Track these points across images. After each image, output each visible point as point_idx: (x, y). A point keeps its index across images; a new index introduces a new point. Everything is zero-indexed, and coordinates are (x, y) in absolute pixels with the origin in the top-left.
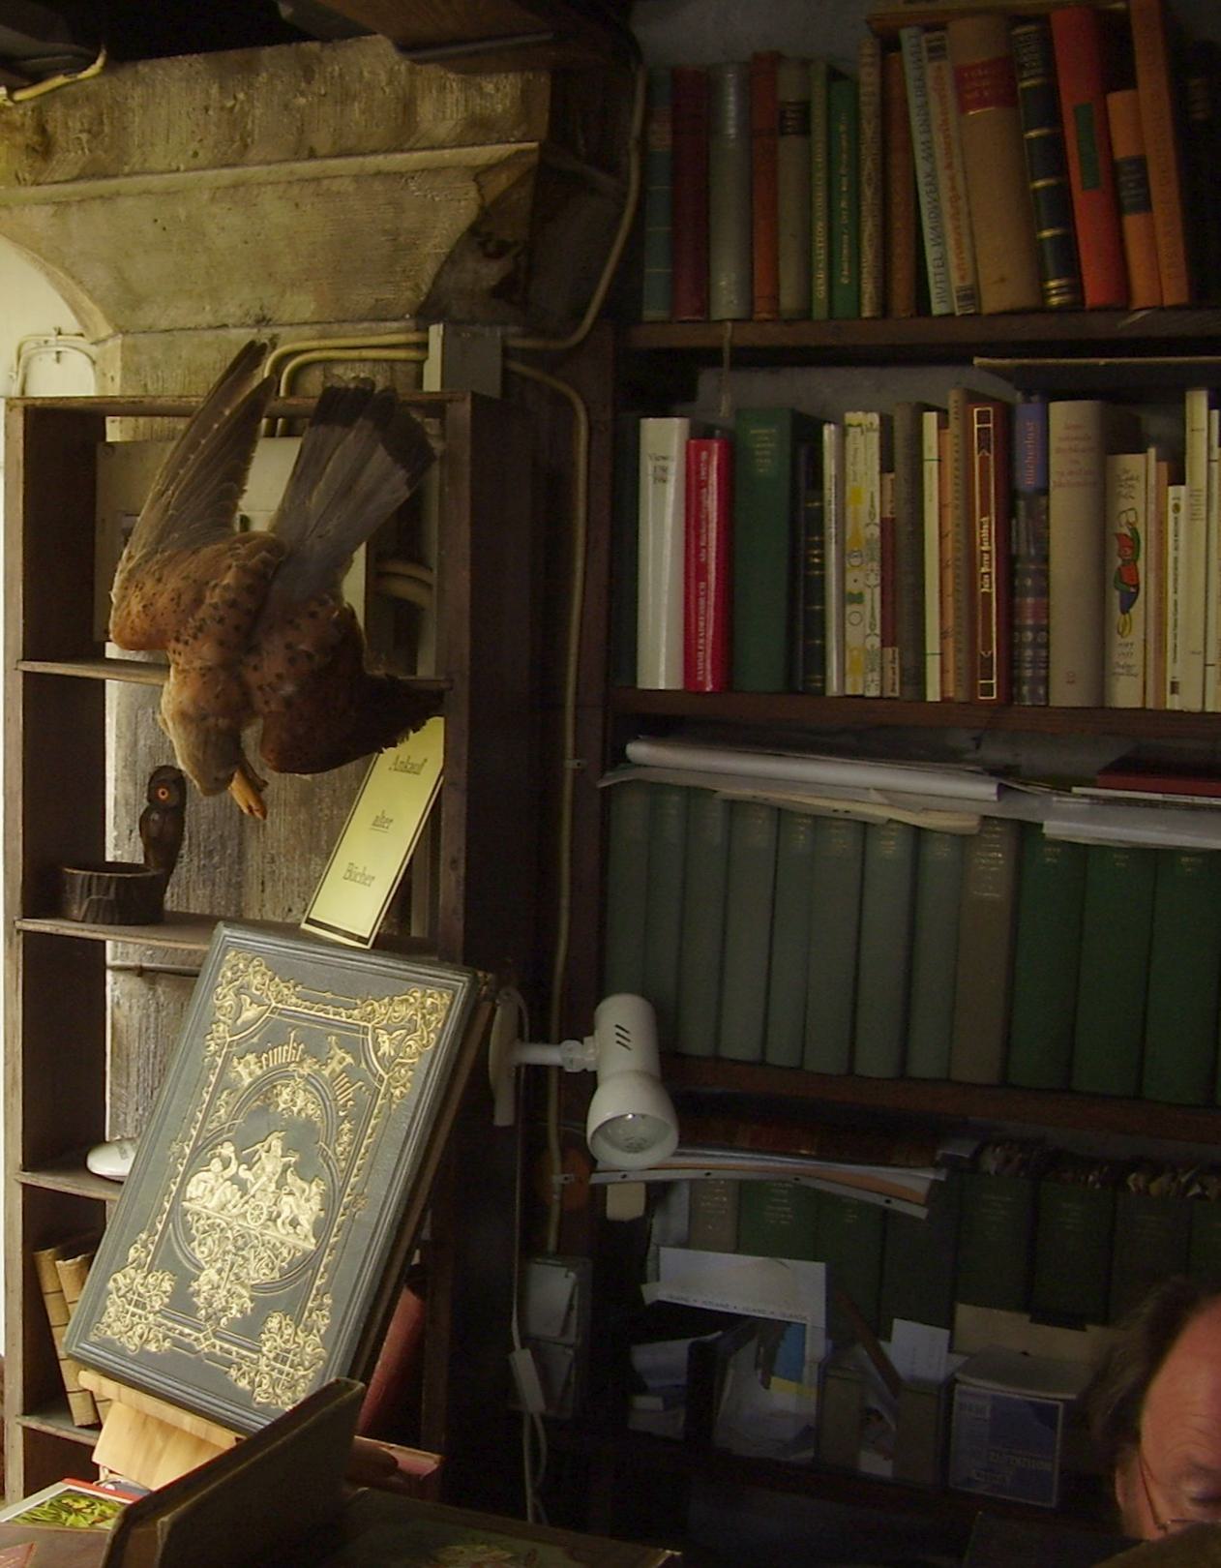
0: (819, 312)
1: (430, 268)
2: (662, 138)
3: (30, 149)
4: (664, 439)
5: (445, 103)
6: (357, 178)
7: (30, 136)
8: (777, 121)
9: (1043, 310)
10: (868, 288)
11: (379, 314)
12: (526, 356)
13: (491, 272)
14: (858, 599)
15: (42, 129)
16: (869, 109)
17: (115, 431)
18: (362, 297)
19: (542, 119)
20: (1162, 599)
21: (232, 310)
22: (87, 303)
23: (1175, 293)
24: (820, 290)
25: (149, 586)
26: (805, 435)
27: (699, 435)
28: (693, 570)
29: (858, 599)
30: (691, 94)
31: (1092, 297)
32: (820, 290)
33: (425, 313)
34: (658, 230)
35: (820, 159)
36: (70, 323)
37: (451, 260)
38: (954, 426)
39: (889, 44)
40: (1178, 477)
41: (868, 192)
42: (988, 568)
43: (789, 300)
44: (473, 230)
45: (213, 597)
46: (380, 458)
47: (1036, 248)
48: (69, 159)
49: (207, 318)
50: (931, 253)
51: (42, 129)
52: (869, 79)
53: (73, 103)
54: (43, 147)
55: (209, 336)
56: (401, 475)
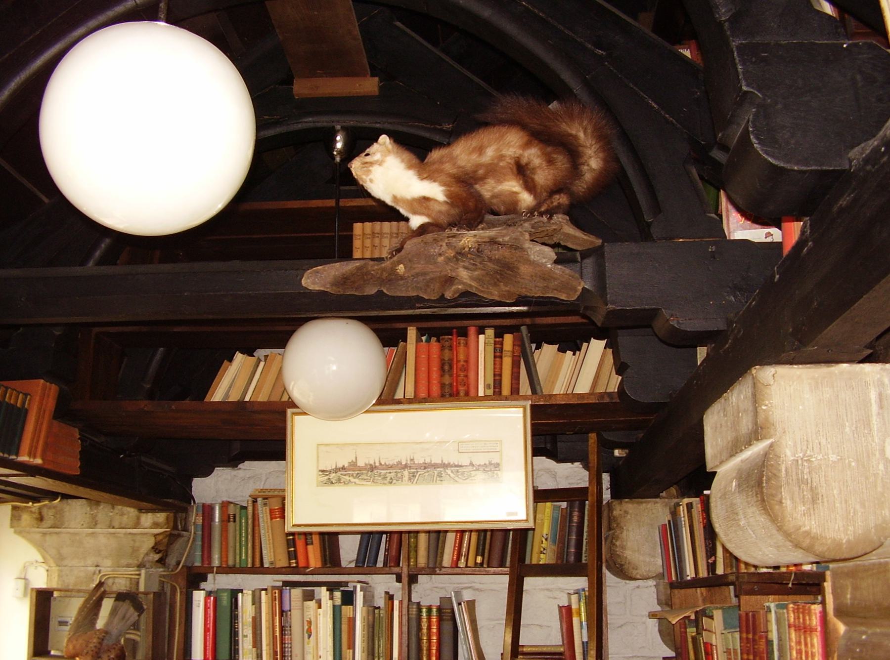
0: (238, 566)
1: (142, 556)
2: (200, 521)
3: (37, 519)
4: (199, 597)
5: (147, 519)
6: (125, 534)
7: (36, 515)
8: (227, 519)
9: (290, 567)
10: (250, 560)
11: (128, 566)
12: (164, 576)
13: (157, 557)
14: (246, 636)
15: (40, 513)
16: (250, 516)
17: (56, 594)
18: (124, 562)
19: (172, 524)
20: (317, 636)
21: (89, 562)
22: (49, 557)
23: (319, 565)
24: (238, 561)
25: (75, 642)
26: (234, 594)
27: (209, 594)
28: (206, 630)
29: (246, 636)
30: (207, 510)
31: (300, 565)
32: (238, 561)
33: (140, 566)
34: (199, 543)
35: (238, 528)
36: (40, 559)
37: (147, 554)
38: (270, 595)
39: (255, 501)
40: (320, 607)
41: (250, 537)
42: (278, 629)
43: (231, 563)
44: (153, 548)
45: (91, 645)
46: (132, 609)
47: (289, 552)
48: (49, 521)
49: (82, 564)
50: (264, 552)
51: (40, 513)
52: (250, 509)
53: (50, 508)
54: (41, 519)
55: (83, 568)
56: (136, 614)
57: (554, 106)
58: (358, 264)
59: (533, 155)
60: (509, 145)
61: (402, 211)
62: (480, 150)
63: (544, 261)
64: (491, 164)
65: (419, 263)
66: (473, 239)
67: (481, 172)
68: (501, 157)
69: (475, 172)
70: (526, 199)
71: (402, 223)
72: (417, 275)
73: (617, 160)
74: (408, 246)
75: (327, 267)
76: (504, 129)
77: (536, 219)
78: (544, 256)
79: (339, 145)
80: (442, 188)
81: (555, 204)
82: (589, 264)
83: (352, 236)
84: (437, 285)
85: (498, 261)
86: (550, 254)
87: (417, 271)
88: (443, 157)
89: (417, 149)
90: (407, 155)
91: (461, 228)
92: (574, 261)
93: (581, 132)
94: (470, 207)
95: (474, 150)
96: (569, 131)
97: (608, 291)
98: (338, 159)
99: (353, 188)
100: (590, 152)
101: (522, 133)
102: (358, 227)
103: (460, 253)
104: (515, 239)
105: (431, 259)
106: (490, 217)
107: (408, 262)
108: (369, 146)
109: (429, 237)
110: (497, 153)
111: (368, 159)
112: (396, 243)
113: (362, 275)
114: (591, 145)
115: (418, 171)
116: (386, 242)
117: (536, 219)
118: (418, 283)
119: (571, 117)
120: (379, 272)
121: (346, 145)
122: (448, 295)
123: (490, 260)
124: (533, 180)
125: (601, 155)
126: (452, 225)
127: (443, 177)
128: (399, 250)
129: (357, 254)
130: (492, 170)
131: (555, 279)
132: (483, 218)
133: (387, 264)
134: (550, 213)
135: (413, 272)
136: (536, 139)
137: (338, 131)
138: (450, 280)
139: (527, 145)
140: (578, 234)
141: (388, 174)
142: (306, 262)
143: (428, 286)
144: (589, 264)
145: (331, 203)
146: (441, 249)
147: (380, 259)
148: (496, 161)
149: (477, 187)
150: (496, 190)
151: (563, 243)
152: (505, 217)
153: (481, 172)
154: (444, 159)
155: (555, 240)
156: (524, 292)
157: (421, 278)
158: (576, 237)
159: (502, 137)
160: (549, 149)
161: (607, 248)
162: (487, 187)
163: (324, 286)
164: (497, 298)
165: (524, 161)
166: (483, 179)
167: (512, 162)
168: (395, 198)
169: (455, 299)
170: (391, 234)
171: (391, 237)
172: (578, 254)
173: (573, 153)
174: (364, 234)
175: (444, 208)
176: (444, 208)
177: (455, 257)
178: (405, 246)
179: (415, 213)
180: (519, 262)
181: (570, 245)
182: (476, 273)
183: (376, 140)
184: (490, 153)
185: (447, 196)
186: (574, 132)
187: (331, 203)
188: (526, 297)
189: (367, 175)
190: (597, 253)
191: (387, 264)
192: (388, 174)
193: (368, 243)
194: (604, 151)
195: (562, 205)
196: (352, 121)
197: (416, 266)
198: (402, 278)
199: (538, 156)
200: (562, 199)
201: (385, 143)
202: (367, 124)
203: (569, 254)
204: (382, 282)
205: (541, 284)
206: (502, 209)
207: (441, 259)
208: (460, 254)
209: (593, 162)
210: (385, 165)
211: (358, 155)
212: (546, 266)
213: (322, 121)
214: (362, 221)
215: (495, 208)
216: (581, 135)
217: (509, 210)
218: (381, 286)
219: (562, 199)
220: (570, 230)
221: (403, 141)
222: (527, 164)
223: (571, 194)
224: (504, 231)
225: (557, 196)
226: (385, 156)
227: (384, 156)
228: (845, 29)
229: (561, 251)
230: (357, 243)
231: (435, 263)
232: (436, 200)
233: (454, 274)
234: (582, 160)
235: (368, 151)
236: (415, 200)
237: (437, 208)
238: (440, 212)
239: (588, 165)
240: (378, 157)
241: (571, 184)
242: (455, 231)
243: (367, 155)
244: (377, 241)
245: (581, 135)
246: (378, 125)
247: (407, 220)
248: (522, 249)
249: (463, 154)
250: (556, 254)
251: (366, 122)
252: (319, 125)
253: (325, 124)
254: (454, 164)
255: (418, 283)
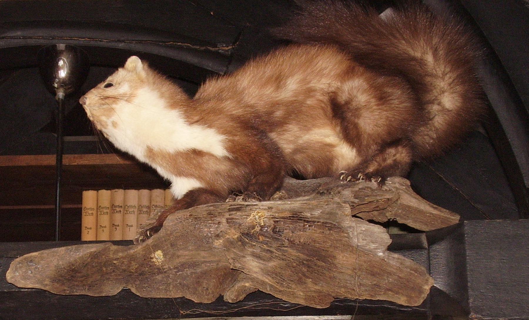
57: (387, 14)
58: (93, 249)
59: (357, 90)
60: (320, 74)
61: (162, 171)
62: (278, 81)
63: (373, 246)
64: (292, 102)
65: (186, 249)
66: (267, 214)
67: (279, 113)
68: (309, 92)
69: (270, 113)
70: (346, 155)
71: (157, 192)
72: (183, 266)
73: (483, 96)
74: (170, 222)
75: (46, 253)
76: (313, 51)
77: (362, 184)
78: (374, 239)
79: (63, 74)
80: (222, 137)
81: (389, 161)
82: (441, 251)
83: (81, 208)
84: (213, 282)
85: (303, 247)
86: (382, 236)
87: (182, 260)
88: (222, 91)
89: (184, 78)
90: (169, 88)
91: (249, 196)
92: (418, 247)
93: (429, 55)
94: (262, 168)
95: (268, 81)
96: (412, 53)
97: (470, 292)
98: (61, 94)
99: (89, 138)
100: (442, 84)
101: (339, 57)
102: (89, 197)
103: (247, 235)
104: (330, 213)
105: (203, 243)
106: (291, 181)
107: (171, 246)
108: (111, 73)
109: (201, 209)
110: (302, 87)
111: (110, 92)
112: (148, 221)
113: (98, 266)
114: (444, 74)
115: (186, 111)
116: (132, 219)
117: (362, 184)
118: (184, 279)
119: (415, 33)
120: (126, 262)
121: (73, 72)
122: (230, 296)
123: (292, 243)
124: (356, 126)
125: (459, 88)
126: (235, 192)
127: (223, 121)
128: (156, 229)
129: (87, 235)
130: (295, 111)
131: (390, 274)
132: (282, 183)
133: (138, 250)
134: (382, 175)
135: (177, 262)
136: (361, 64)
137: (61, 52)
138: (232, 274)
139: (348, 74)
140: (425, 206)
141: (138, 113)
142: (11, 245)
143: (198, 283)
144: (441, 251)
145: (50, 160)
146: (219, 228)
147: (127, 243)
148: (301, 98)
149: (273, 135)
150: (301, 142)
151: (400, 221)
152: (314, 181)
153: (279, 113)
154: (224, 94)
155: (389, 215)
156: (343, 293)
157: (188, 271)
158: (422, 212)
159: (310, 61)
160: (381, 80)
161: (468, 227)
162: (287, 136)
163: (41, 283)
164: (302, 302)
165: (343, 98)
166: (281, 123)
167: (325, 99)
168: (150, 151)
169: (239, 303)
170: (140, 206)
171: (140, 212)
172: (424, 239)
173: (417, 87)
174: (98, 208)
175: (224, 167)
176: (224, 167)
177: (240, 239)
178: (166, 223)
179: (180, 173)
180: (336, 248)
181: (411, 223)
182: (271, 264)
183: (122, 64)
184: (292, 86)
185: (230, 149)
186: (418, 55)
187: (50, 160)
188: (346, 300)
189: (109, 116)
190: (453, 235)
191: (138, 250)
192: (138, 113)
193: (105, 220)
194: (463, 83)
195: (400, 163)
196: (83, 38)
197: (181, 252)
198: (160, 271)
199: (365, 91)
200: (400, 155)
201: (135, 69)
202: (104, 43)
203: (411, 236)
204: (128, 276)
205: (368, 281)
206: (310, 168)
207: (218, 243)
208: (248, 236)
209: (447, 100)
210: (136, 101)
211: (94, 85)
212: (375, 255)
213: (38, 37)
214: (96, 187)
215: (299, 167)
216: (429, 58)
217: (321, 173)
218: (127, 282)
219: (400, 155)
220: (411, 200)
221: (162, 67)
222: (348, 103)
223: (413, 147)
224: (314, 202)
225: (392, 151)
226: (136, 88)
227: (135, 88)
228: (115, 243)
229: (395, 231)
230: (88, 221)
231: (211, 248)
232: (211, 155)
233: (238, 265)
234: (430, 97)
235: (109, 79)
236: (179, 154)
237: (212, 166)
238: (218, 173)
239: (439, 104)
240: (124, 89)
241: (413, 132)
242: (239, 200)
243: (109, 85)
244: (118, 217)
245: (429, 58)
246: (121, 45)
247: (166, 185)
248: (340, 229)
249: (252, 86)
250: (392, 236)
251: (105, 40)
252: (32, 42)
253: (42, 42)
254: (239, 102)
255: (184, 279)
